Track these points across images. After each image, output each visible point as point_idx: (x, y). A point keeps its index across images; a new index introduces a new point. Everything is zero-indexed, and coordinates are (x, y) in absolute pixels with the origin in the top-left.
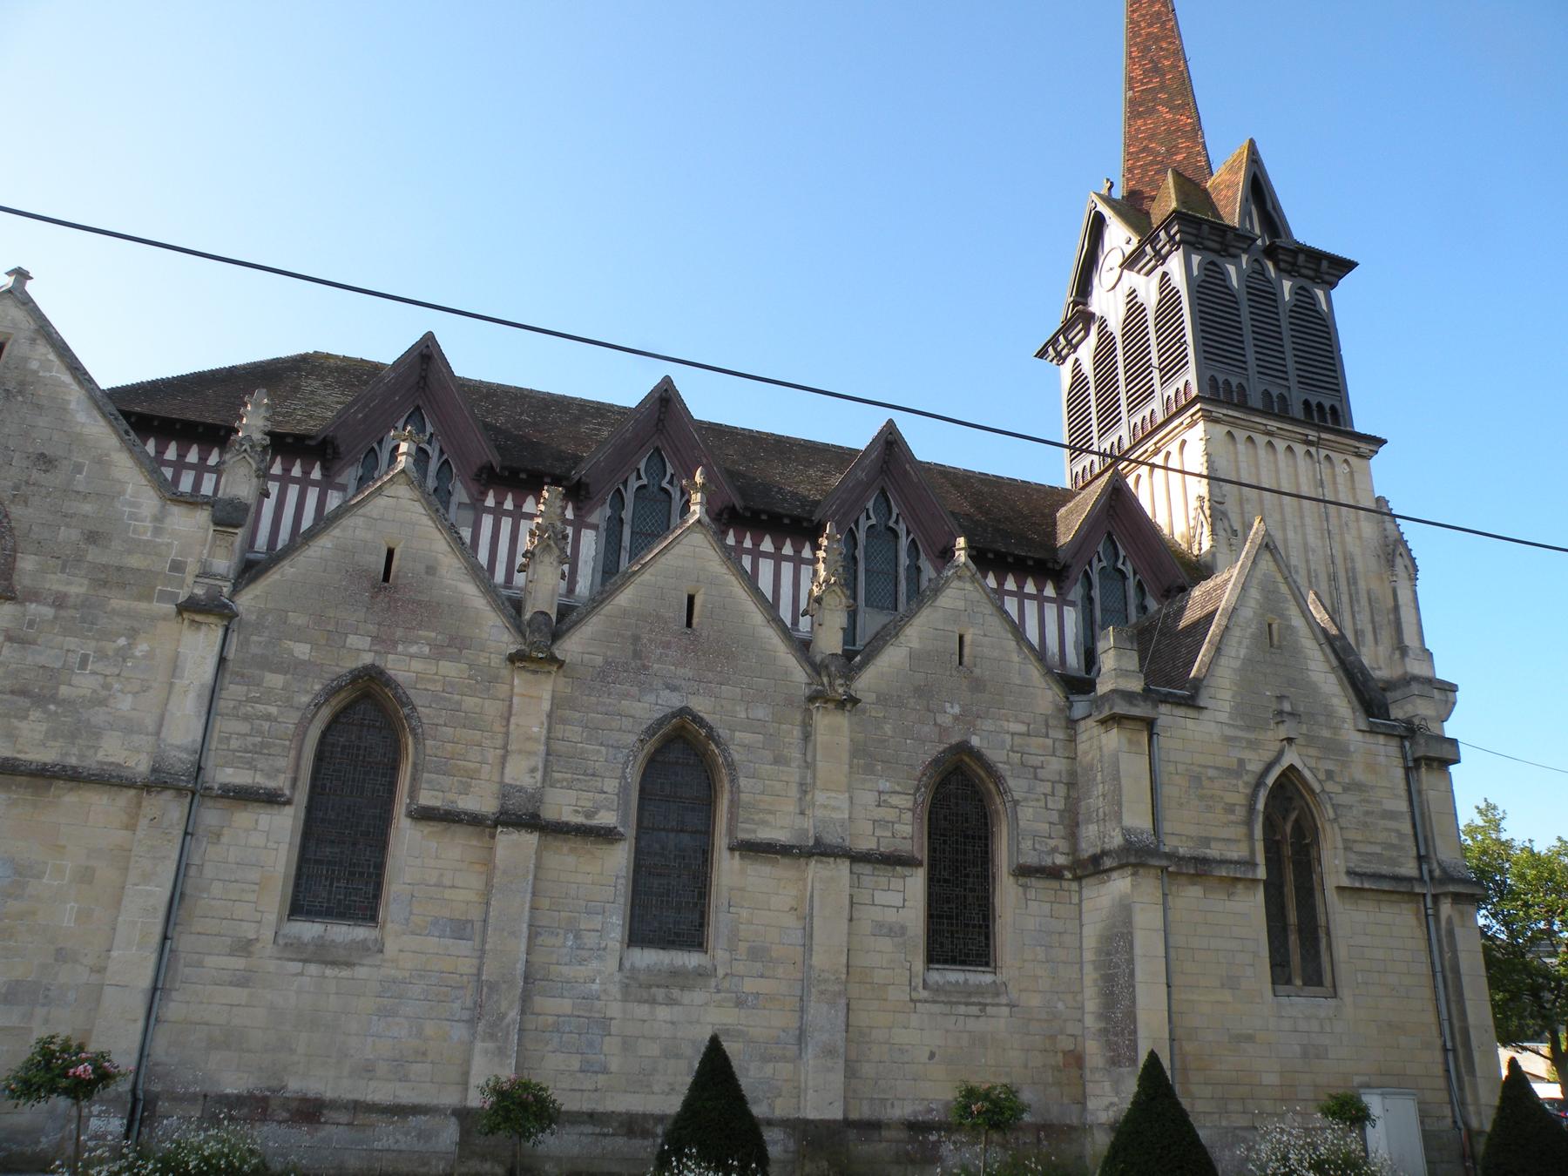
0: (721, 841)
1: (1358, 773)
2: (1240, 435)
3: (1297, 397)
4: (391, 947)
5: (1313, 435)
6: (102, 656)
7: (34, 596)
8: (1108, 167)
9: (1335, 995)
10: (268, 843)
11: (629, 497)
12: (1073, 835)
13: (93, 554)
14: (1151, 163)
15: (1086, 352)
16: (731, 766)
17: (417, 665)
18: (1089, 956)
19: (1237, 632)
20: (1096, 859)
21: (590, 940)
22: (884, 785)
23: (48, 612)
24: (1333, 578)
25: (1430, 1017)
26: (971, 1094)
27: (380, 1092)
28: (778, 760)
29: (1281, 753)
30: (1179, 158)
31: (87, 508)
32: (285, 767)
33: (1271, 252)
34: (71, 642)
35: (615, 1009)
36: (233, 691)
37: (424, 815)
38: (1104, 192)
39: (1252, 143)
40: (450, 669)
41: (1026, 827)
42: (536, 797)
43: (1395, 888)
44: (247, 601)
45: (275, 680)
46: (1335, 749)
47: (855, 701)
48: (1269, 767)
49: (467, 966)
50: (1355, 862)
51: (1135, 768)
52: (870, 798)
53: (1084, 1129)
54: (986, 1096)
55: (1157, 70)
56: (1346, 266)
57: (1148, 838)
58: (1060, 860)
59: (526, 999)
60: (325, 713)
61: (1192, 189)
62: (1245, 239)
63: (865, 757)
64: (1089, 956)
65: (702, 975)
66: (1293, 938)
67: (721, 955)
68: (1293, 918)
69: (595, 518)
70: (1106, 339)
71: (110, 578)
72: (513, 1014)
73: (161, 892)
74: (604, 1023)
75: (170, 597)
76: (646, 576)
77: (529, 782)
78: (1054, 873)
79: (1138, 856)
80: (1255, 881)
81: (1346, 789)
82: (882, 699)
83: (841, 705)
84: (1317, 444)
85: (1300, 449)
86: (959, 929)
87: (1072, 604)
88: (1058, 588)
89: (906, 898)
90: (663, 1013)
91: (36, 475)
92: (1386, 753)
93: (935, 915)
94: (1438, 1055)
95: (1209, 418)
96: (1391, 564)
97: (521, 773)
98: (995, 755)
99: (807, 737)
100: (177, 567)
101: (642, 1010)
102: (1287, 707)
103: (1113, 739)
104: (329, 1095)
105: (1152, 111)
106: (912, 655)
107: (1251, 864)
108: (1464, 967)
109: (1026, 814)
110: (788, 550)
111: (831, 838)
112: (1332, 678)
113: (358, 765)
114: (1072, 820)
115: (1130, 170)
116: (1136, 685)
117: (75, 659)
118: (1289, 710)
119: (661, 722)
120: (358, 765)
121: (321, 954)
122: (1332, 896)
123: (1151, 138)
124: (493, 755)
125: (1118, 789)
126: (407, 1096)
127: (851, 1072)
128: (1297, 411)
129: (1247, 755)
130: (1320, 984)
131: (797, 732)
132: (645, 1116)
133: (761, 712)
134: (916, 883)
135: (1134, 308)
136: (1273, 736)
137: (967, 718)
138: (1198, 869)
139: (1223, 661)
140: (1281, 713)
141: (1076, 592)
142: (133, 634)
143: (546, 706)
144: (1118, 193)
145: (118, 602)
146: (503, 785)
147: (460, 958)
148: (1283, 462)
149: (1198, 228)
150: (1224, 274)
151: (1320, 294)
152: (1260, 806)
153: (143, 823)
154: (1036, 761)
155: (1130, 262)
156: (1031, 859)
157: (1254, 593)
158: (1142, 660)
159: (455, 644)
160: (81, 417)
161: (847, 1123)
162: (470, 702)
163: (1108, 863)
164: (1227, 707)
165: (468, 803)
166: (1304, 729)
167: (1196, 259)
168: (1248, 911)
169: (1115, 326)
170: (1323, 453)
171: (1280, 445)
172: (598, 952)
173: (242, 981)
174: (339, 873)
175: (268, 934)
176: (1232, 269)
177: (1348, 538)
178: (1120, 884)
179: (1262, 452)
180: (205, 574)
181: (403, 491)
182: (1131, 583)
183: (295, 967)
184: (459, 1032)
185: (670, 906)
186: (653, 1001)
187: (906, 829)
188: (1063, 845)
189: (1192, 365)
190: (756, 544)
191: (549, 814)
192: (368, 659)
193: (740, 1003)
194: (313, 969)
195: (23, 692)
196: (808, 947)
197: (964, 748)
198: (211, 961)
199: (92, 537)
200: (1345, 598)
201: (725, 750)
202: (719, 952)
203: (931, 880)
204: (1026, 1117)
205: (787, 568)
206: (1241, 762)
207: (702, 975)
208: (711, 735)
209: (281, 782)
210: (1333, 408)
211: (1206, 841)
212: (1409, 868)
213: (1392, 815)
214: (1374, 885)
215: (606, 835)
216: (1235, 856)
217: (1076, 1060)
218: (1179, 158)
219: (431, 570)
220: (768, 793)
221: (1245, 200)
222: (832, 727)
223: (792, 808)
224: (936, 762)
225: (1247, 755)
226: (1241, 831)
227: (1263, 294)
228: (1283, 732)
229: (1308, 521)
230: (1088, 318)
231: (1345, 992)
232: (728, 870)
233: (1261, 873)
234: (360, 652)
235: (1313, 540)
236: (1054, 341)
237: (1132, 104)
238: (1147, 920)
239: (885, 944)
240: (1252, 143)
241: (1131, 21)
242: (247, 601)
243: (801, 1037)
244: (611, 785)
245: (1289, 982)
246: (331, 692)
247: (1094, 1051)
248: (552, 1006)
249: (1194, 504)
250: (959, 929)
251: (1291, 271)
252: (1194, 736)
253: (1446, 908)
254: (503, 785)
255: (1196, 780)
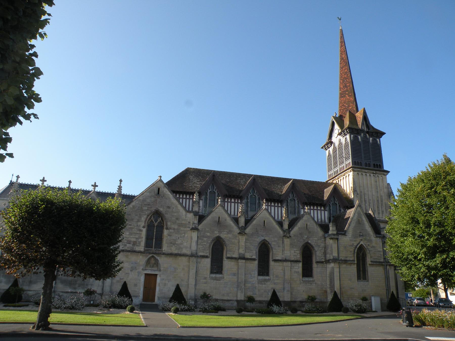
0: (271, 259)
1: (374, 244)
2: (360, 173)
3: (372, 164)
4: (225, 277)
5: (375, 172)
6: (181, 237)
7: (170, 229)
8: (336, 111)
9: (368, 281)
10: (207, 263)
11: (249, 197)
12: (325, 256)
13: (177, 222)
14: (345, 109)
15: (331, 149)
16: (272, 248)
17: (225, 235)
18: (328, 275)
19: (353, 222)
20: (329, 260)
21: (253, 275)
22: (295, 249)
23: (173, 231)
24: (378, 201)
25: (384, 285)
26: (309, 297)
27: (226, 298)
28: (279, 246)
29: (360, 242)
30: (350, 108)
31: (175, 214)
32: (208, 252)
33: (368, 132)
34: (177, 235)
35: (257, 285)
36: (200, 241)
37: (228, 258)
38: (334, 115)
39: (364, 108)
40: (230, 235)
41: (318, 255)
42: (244, 255)
43: (379, 264)
44: (200, 227)
45: (205, 239)
46: (370, 241)
47: (290, 236)
48: (358, 244)
49: (236, 280)
50: (372, 260)
51: (335, 246)
52: (293, 252)
53: (327, 302)
54: (311, 297)
55: (346, 86)
56: (384, 134)
57: (337, 257)
58: (323, 260)
59: (245, 284)
60: (213, 244)
61: (353, 118)
62: (362, 131)
63: (292, 245)
64: (328, 275)
65: (269, 280)
66: (361, 272)
67: (272, 277)
68: (361, 269)
69: (244, 202)
70: (335, 147)
71: (181, 225)
72: (243, 287)
73: (194, 271)
74: (256, 287)
75: (189, 227)
76: (257, 218)
77: (243, 252)
78: (322, 262)
79: (335, 260)
80: (355, 263)
81: (371, 247)
82: (294, 236)
83: (288, 237)
84: (376, 174)
85: (372, 175)
86: (307, 272)
87: (327, 211)
88: (324, 208)
89: (299, 267)
90: (264, 286)
91: (168, 210)
92: (379, 241)
93: (304, 269)
94: (385, 291)
95: (353, 171)
96: (390, 197)
97: (241, 251)
98: (313, 244)
99: (283, 243)
100: (189, 222)
101: (261, 285)
102: (361, 234)
103: (331, 241)
104: (219, 298)
105: (345, 96)
106: (299, 228)
107: (354, 261)
108: (390, 276)
109: (318, 253)
110: (276, 205)
111: (287, 259)
112: (370, 228)
113: (218, 250)
114: (325, 253)
115: (340, 110)
116: (335, 232)
117: (177, 238)
118: (362, 235)
119: (261, 242)
120: (218, 250)
121: (216, 279)
122: (368, 265)
123: (345, 102)
124: (237, 248)
125: (332, 250)
126: (229, 298)
127: (291, 294)
128: (372, 165)
129: (354, 243)
130: (366, 279)
131: (281, 242)
132: (262, 301)
133: (276, 239)
134: (300, 265)
135: (340, 143)
136: (359, 239)
137: (308, 238)
138: (345, 262)
139: (350, 227)
140: (360, 235)
141: (327, 208)
142: (185, 233)
143: (244, 240)
144: (337, 116)
145: (182, 229)
146: (239, 253)
147: (235, 278)
148: (369, 179)
149: (353, 130)
150: (358, 138)
151: (378, 140)
152: (356, 251)
153: (191, 262)
154: (319, 244)
155: (340, 134)
156: (318, 260)
157: (356, 214)
158: (336, 228)
159: (230, 232)
160: (172, 200)
161: (291, 301)
162: (233, 240)
163: (330, 261)
164: (351, 235)
165: (234, 256)
166: (364, 237)
167: (352, 136)
168: (354, 268)
169: (337, 144)
170: (377, 175)
171: (368, 174)
172: (254, 278)
173: (206, 283)
174: (217, 267)
175: (208, 276)
176: (359, 137)
177: (381, 192)
178: (332, 265)
179: (364, 176)
180: (194, 223)
181: (220, 208)
182: (338, 205)
183: (213, 281)
184: (236, 289)
185: (264, 270)
186: (262, 284)
187: (299, 256)
188: (324, 258)
189: (351, 159)
190: (271, 204)
191: (246, 257)
192: (218, 235)
193: (275, 284)
194: (215, 281)
195: (171, 243)
196: (284, 275)
197: (308, 243)
198: (201, 280)
199: (177, 219)
200: (380, 205)
201: (271, 246)
202: (271, 276)
203: (303, 264)
204: (317, 300)
205: (276, 208)
206: (353, 244)
207: (269, 280)
208: (269, 243)
209: (208, 254)
210: (380, 165)
211: (347, 257)
212: (382, 260)
213: (380, 251)
214: (376, 263)
215: (254, 260)
216: (351, 259)
217: (326, 292)
218: (350, 108)
219: (226, 220)
220: (277, 252)
221: (363, 121)
222: (287, 241)
223: (281, 254)
224: (303, 245)
225: (354, 243)
226: (352, 255)
227: (366, 141)
228: (360, 238)
229: (373, 190)
230: (331, 143)
231: (370, 281)
232: (272, 263)
233: (356, 262)
234: (217, 234)
235: (374, 194)
236: (325, 146)
237: (341, 94)
238: (336, 270)
239: (296, 274)
240: (364, 108)
241: (341, 74)
242: (200, 227)
243: (284, 289)
244: (254, 252)
245: (360, 279)
246: (213, 240)
247: (329, 290)
248: (248, 285)
249: (350, 188)
250: (307, 272)
251: (371, 135)
252: (344, 240)
253: (388, 267)
254: (239, 253)
255: (345, 247)
